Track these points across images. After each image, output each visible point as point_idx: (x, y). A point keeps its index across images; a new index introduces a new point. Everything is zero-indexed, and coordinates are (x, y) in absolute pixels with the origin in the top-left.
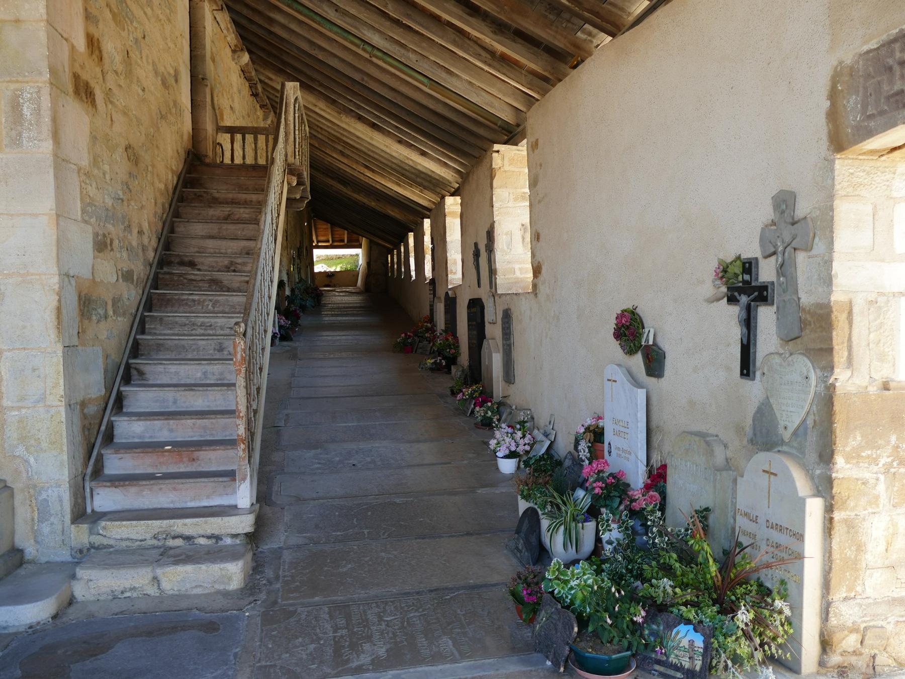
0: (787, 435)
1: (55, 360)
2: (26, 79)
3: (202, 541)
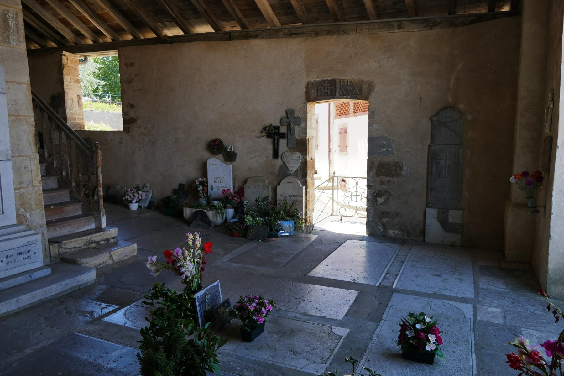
0: (292, 173)
1: (36, 162)
2: (10, 5)
3: (102, 242)
